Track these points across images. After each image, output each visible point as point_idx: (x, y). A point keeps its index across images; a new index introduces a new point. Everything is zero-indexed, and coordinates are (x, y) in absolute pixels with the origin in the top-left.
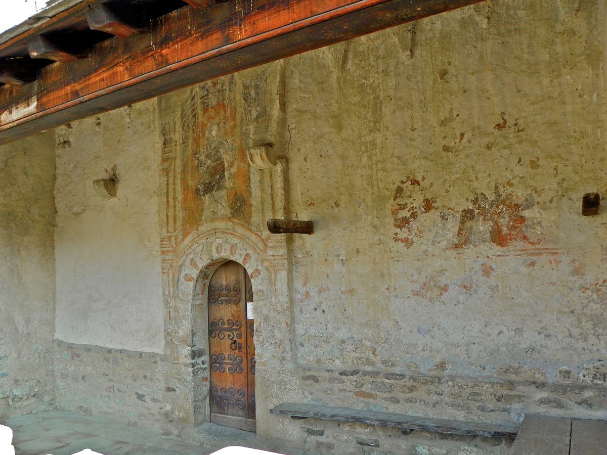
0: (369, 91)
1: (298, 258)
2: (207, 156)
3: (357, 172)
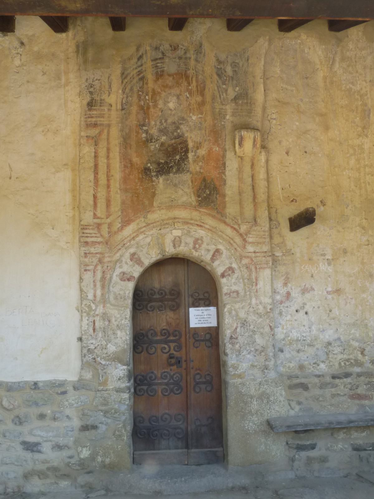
0: (357, 97)
1: (276, 256)
2: (160, 131)
3: (345, 173)
